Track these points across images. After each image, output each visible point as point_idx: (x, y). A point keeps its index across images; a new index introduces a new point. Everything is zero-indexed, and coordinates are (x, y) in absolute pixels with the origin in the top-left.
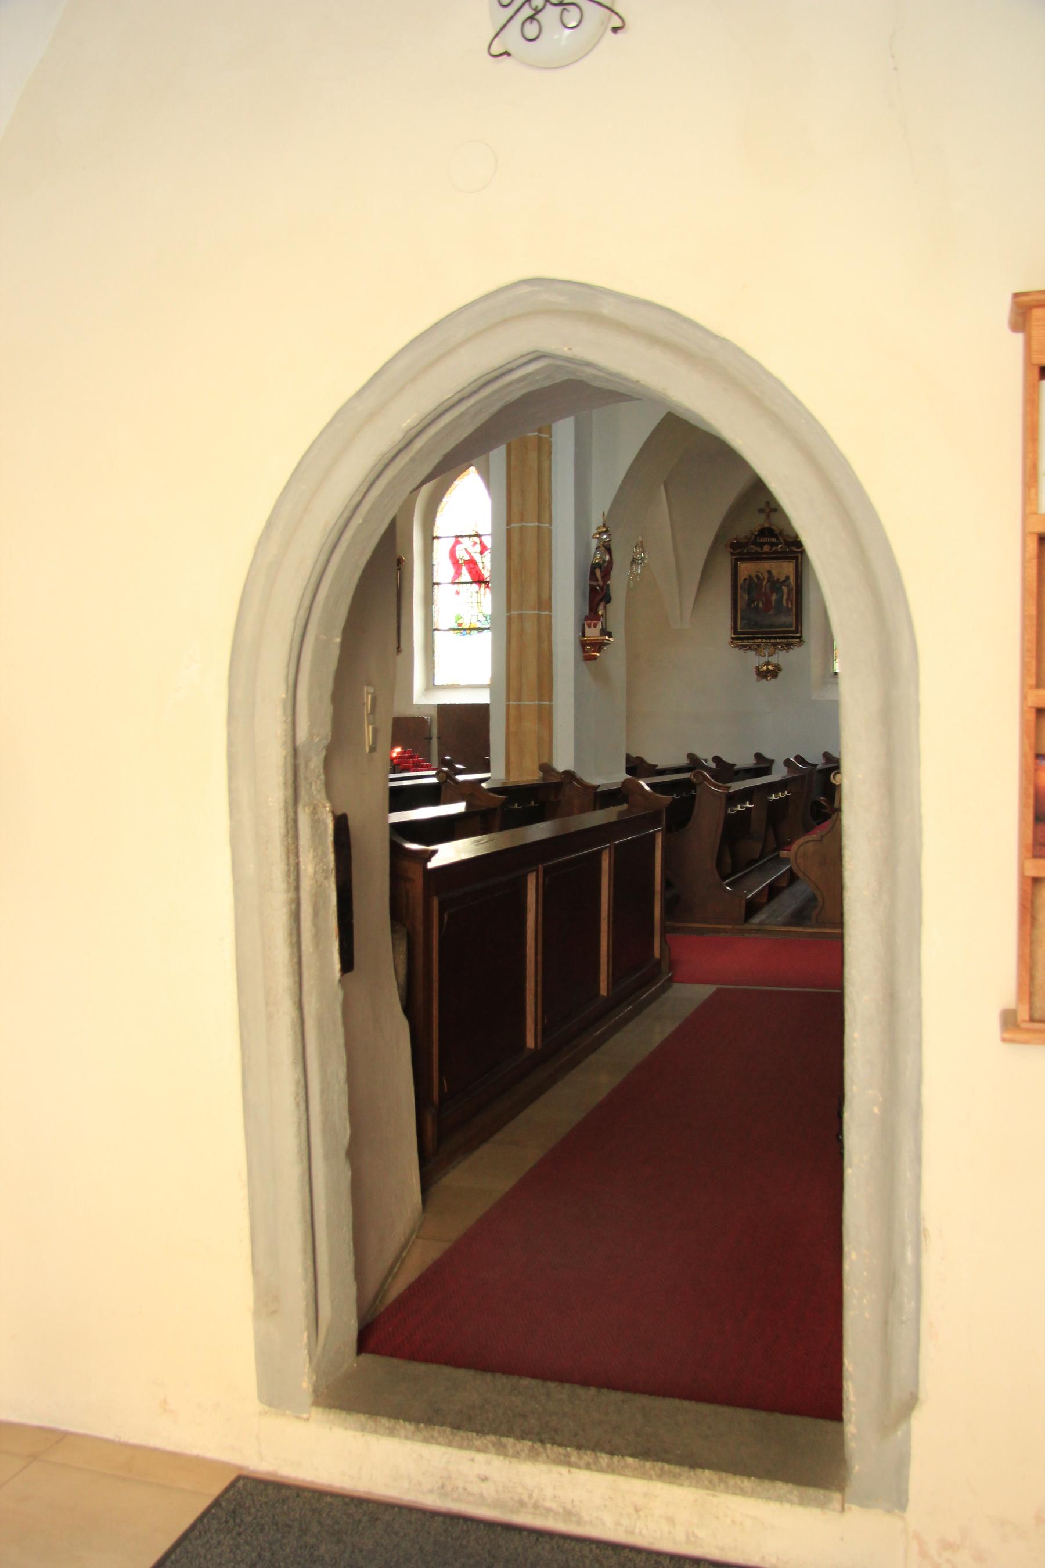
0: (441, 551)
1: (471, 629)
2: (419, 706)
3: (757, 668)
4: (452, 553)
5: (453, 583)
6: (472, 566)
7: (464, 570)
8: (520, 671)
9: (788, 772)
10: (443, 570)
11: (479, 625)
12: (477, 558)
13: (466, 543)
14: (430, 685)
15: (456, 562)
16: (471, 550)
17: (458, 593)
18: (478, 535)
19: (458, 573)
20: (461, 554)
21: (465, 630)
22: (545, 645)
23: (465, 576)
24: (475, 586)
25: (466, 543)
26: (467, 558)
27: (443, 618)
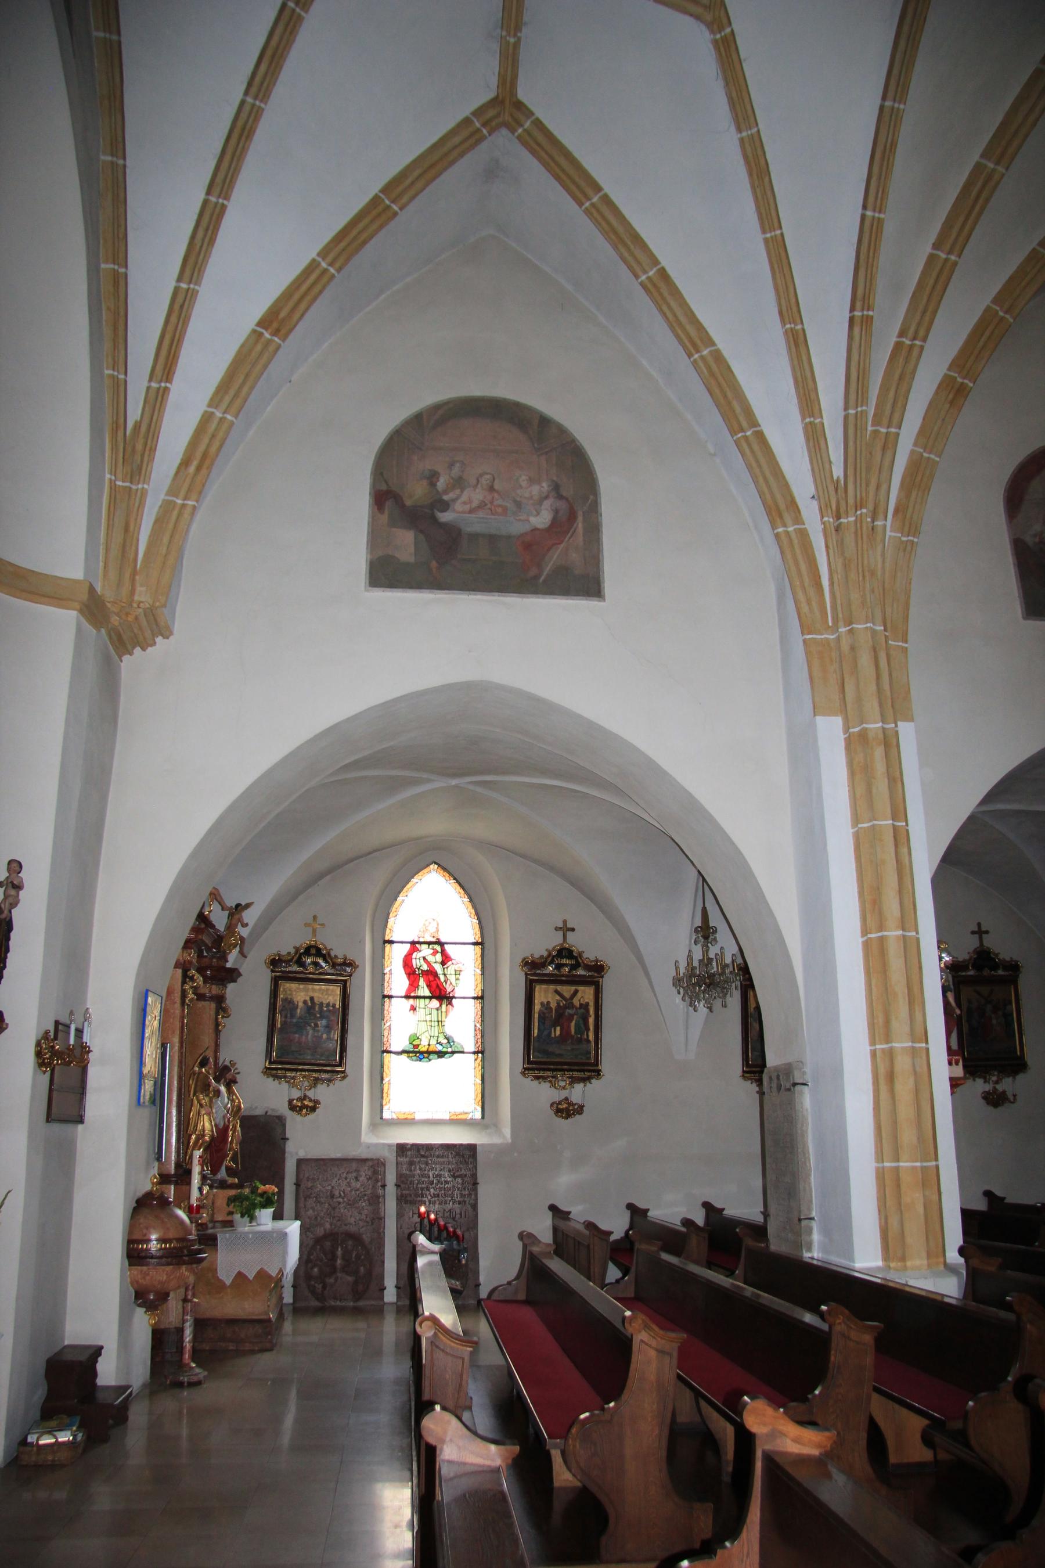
0: (396, 955)
1: (429, 1053)
2: (368, 1146)
3: (290, 1102)
4: (407, 962)
5: (407, 997)
6: (431, 979)
7: (422, 982)
8: (291, 33)
9: (965, 1297)
10: (398, 982)
11: (440, 1048)
12: (438, 968)
13: (425, 951)
14: (379, 1121)
15: (411, 973)
16: (431, 959)
17: (413, 1009)
18: (438, 942)
19: (414, 985)
20: (417, 962)
21: (422, 1053)
22: (860, 790)
23: (424, 990)
24: (435, 1003)
25: (425, 951)
26: (425, 967)
27: (398, 1040)
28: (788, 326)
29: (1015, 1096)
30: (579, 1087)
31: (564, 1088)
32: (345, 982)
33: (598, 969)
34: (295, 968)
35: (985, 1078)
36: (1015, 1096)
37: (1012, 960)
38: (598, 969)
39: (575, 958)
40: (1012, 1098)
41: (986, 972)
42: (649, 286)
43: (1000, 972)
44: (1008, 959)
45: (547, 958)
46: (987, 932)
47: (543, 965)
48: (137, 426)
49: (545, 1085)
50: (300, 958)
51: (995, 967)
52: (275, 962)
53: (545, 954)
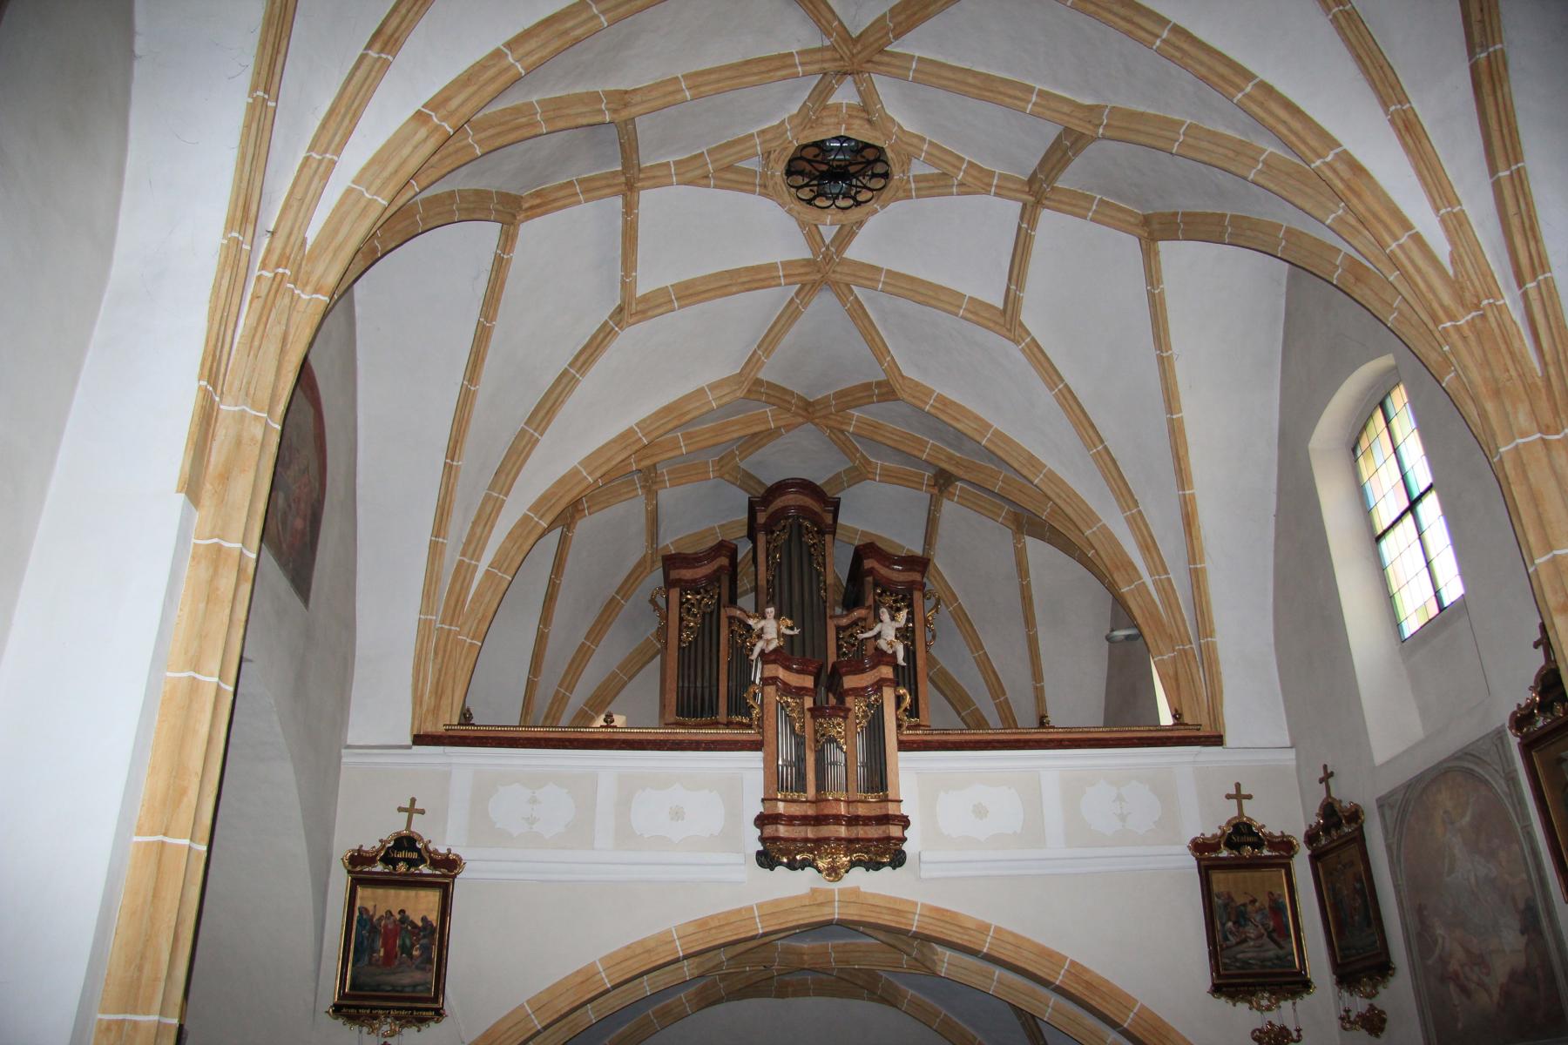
28: (1392, 108)
29: (1298, 1031)
30: (1286, 1005)
31: (1269, 1009)
32: (447, 885)
33: (450, 864)
34: (379, 868)
35: (1250, 1002)
36: (1298, 1031)
37: (1283, 835)
38: (450, 864)
39: (418, 851)
40: (1295, 1035)
41: (1247, 851)
42: (1238, 80)
43: (1266, 852)
44: (1277, 834)
45: (379, 851)
46: (1249, 797)
47: (371, 860)
48: (1455, 259)
49: (1243, 1007)
50: (387, 853)
51: (1258, 843)
52: (357, 860)
53: (378, 845)
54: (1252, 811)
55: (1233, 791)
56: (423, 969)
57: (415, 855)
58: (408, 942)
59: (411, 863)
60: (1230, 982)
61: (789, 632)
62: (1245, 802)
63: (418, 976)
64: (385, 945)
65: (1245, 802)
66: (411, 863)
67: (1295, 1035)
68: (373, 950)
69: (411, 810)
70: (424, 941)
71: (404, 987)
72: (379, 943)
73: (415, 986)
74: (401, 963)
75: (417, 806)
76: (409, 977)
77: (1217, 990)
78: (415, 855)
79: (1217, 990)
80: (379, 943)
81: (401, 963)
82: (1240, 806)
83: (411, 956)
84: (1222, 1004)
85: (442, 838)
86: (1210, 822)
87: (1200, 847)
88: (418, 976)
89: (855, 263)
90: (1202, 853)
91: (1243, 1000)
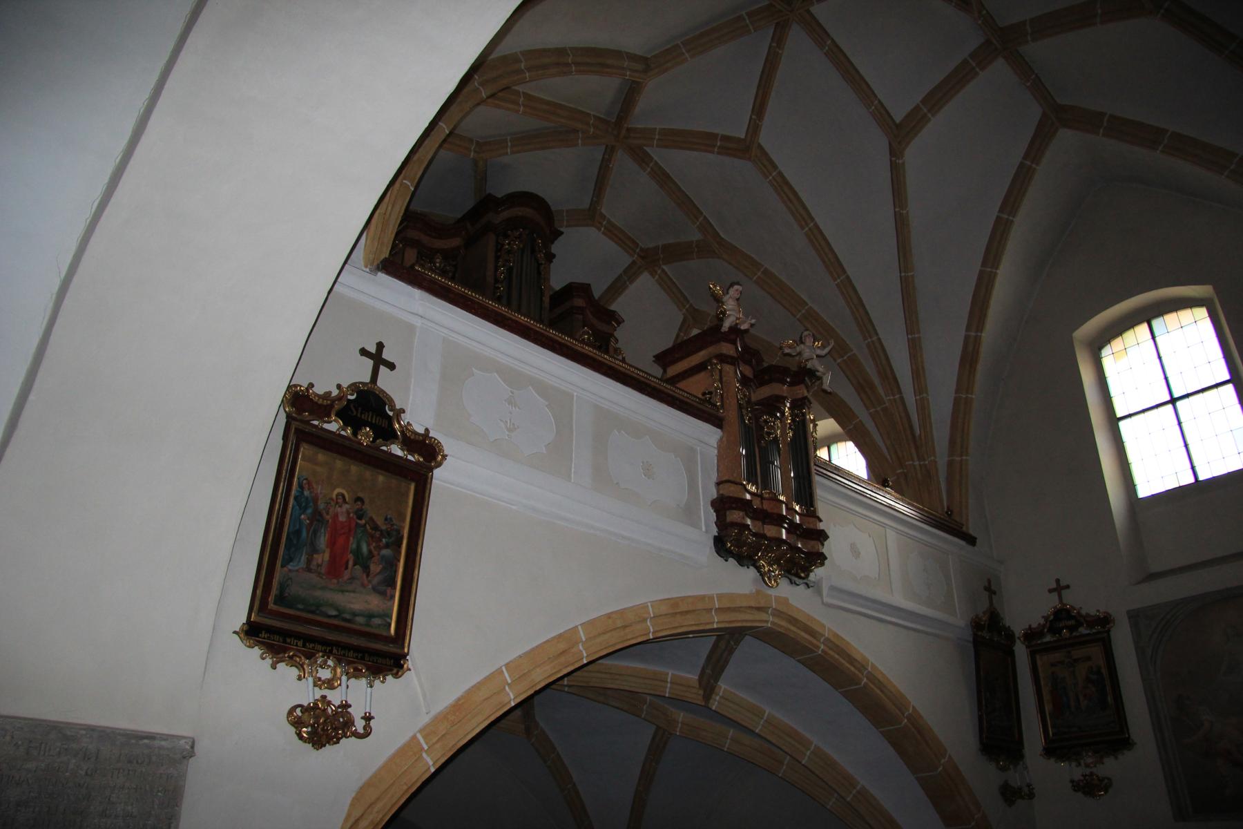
29: (368, 718)
36: (368, 718)
41: (366, 437)
49: (287, 672)
51: (386, 433)
54: (1070, 599)
55: (1063, 583)
56: (383, 594)
57: (1072, 622)
58: (365, 549)
59: (1072, 629)
60: (278, 626)
61: (827, 350)
62: (383, 370)
63: (374, 602)
64: (332, 543)
65: (383, 370)
66: (1072, 629)
67: (359, 725)
68: (314, 550)
69: (1059, 588)
70: (385, 552)
71: (355, 614)
72: (322, 541)
73: (371, 616)
74: (352, 578)
75: (373, 350)
76: (359, 601)
77: (252, 632)
78: (1072, 622)
79: (252, 632)
80: (322, 541)
81: (352, 578)
82: (1060, 596)
83: (366, 569)
84: (253, 658)
85: (418, 409)
86: (338, 374)
87: (300, 403)
88: (374, 602)
89: (907, 116)
90: (300, 410)
91: (292, 662)
